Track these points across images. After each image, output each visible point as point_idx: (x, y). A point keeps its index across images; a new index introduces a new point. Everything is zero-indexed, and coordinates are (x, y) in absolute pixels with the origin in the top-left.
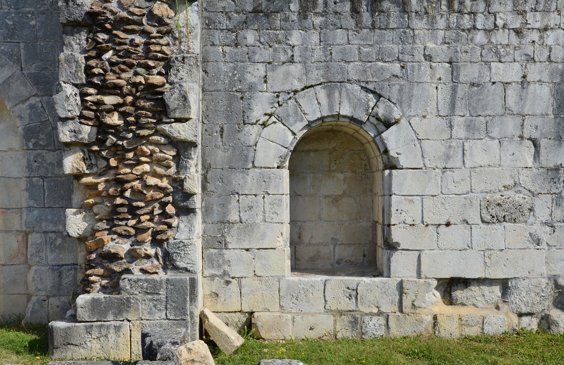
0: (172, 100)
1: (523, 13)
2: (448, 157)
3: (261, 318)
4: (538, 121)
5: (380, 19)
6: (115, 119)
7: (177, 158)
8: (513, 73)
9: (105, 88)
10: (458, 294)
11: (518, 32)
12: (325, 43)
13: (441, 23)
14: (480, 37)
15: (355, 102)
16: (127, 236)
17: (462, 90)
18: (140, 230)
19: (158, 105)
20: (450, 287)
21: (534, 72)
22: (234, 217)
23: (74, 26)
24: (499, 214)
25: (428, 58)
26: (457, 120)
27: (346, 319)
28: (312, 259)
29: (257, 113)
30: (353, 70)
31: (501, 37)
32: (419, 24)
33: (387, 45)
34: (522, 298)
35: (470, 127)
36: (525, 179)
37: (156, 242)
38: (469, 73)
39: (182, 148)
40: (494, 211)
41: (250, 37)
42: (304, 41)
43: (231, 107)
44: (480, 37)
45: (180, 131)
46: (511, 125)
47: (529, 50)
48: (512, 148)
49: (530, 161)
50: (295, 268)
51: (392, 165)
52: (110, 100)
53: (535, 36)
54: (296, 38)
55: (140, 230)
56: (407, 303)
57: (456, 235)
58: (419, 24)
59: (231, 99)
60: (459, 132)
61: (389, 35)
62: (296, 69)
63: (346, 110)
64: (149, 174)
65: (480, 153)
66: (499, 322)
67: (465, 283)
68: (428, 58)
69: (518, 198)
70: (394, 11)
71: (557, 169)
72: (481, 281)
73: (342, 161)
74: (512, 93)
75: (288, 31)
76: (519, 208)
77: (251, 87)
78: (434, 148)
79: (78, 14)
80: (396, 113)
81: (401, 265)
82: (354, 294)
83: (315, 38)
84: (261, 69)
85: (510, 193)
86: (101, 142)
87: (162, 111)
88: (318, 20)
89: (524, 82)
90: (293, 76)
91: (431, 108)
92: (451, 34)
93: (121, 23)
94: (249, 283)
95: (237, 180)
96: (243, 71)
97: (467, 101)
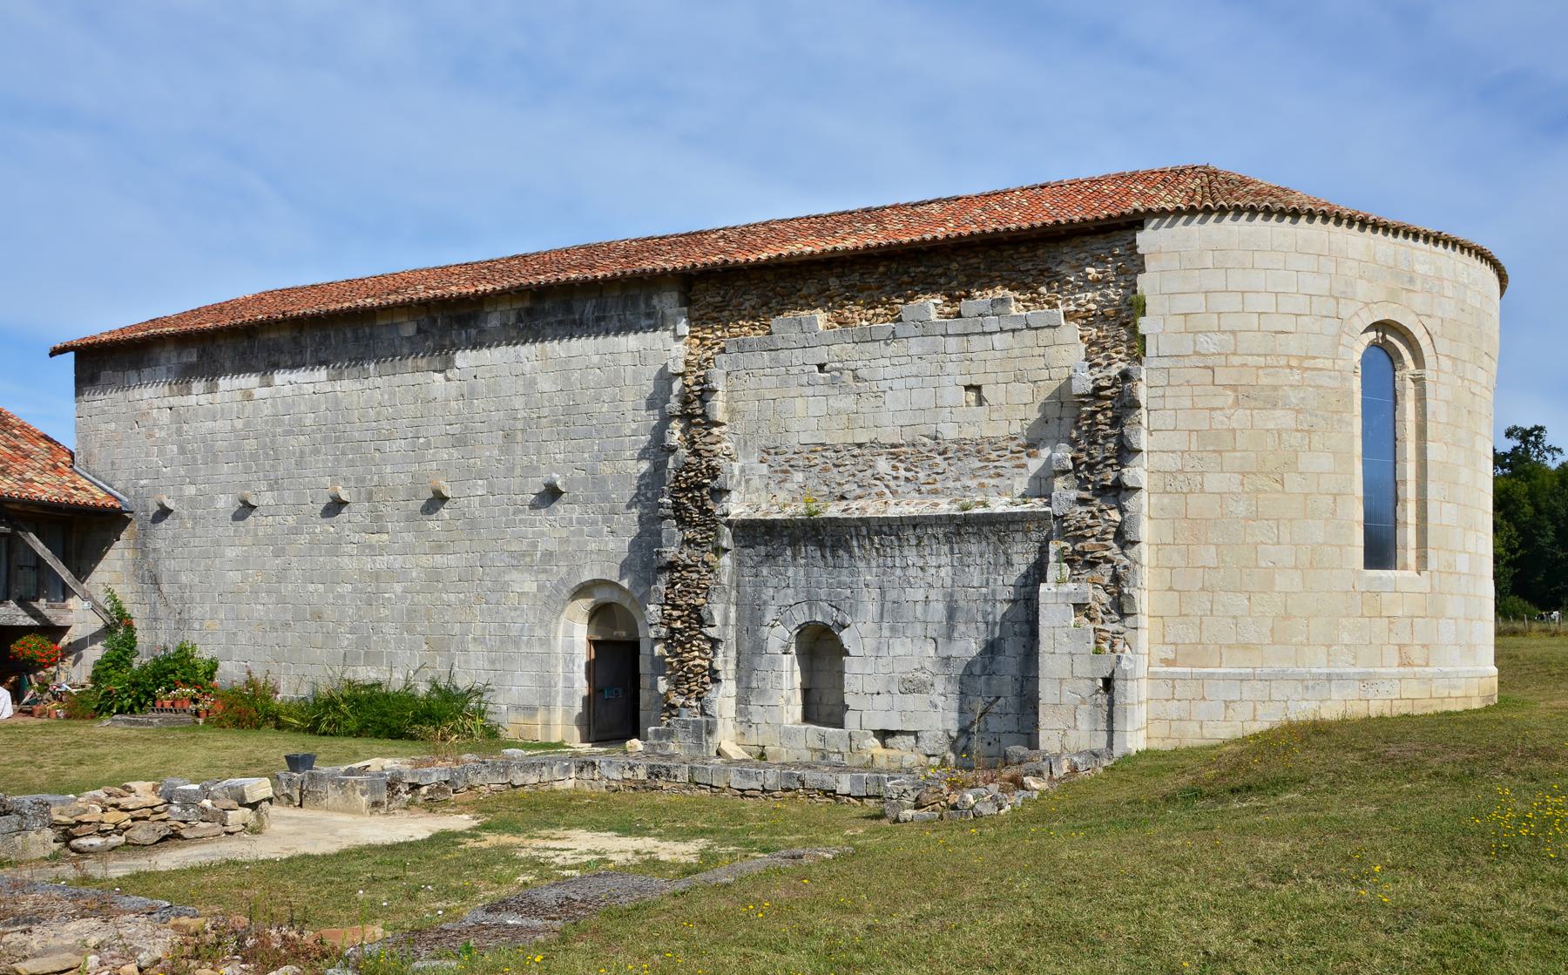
0: (704, 614)
1: (923, 557)
2: (878, 649)
3: (769, 749)
4: (937, 626)
5: (838, 562)
6: (678, 625)
7: (712, 648)
8: (920, 595)
9: (675, 607)
10: (889, 741)
11: (922, 569)
12: (807, 575)
13: (874, 563)
14: (898, 572)
15: (824, 614)
16: (682, 694)
17: (888, 605)
18: (690, 691)
19: (698, 618)
20: (884, 735)
21: (933, 595)
22: (754, 685)
23: (661, 569)
24: (912, 687)
25: (867, 586)
26: (885, 625)
27: (819, 754)
28: (829, 715)
29: (768, 619)
30: (823, 593)
31: (912, 572)
32: (861, 565)
33: (843, 578)
34: (927, 744)
35: (893, 629)
36: (927, 664)
37: (698, 699)
38: (892, 595)
39: (714, 643)
40: (907, 685)
41: (765, 571)
42: (796, 574)
43: (751, 618)
44: (898, 572)
45: (712, 632)
46: (919, 628)
47: (930, 580)
48: (919, 643)
49: (932, 652)
50: (807, 717)
51: (847, 653)
52: (676, 613)
53: (933, 571)
54: (791, 572)
55: (690, 691)
56: (854, 746)
57: (882, 701)
58: (861, 565)
59: (753, 610)
60: (886, 632)
61: (845, 572)
62: (790, 591)
63: (819, 618)
64: (696, 659)
65: (900, 647)
66: (911, 759)
67: (893, 733)
68: (867, 586)
69: (923, 677)
70: (846, 556)
71: (948, 658)
72: (902, 733)
73: (820, 648)
74: (919, 608)
75: (786, 567)
76: (924, 684)
77: (765, 603)
78: (870, 642)
79: (663, 563)
80: (849, 620)
81: (851, 719)
82: (823, 738)
83: (802, 573)
84: (771, 591)
85: (919, 674)
86: (672, 638)
87: (701, 621)
88: (803, 561)
89: (927, 600)
90: (789, 596)
91: (869, 617)
92: (881, 570)
93: (686, 567)
94: (762, 727)
95: (756, 660)
96: (760, 592)
97: (893, 615)
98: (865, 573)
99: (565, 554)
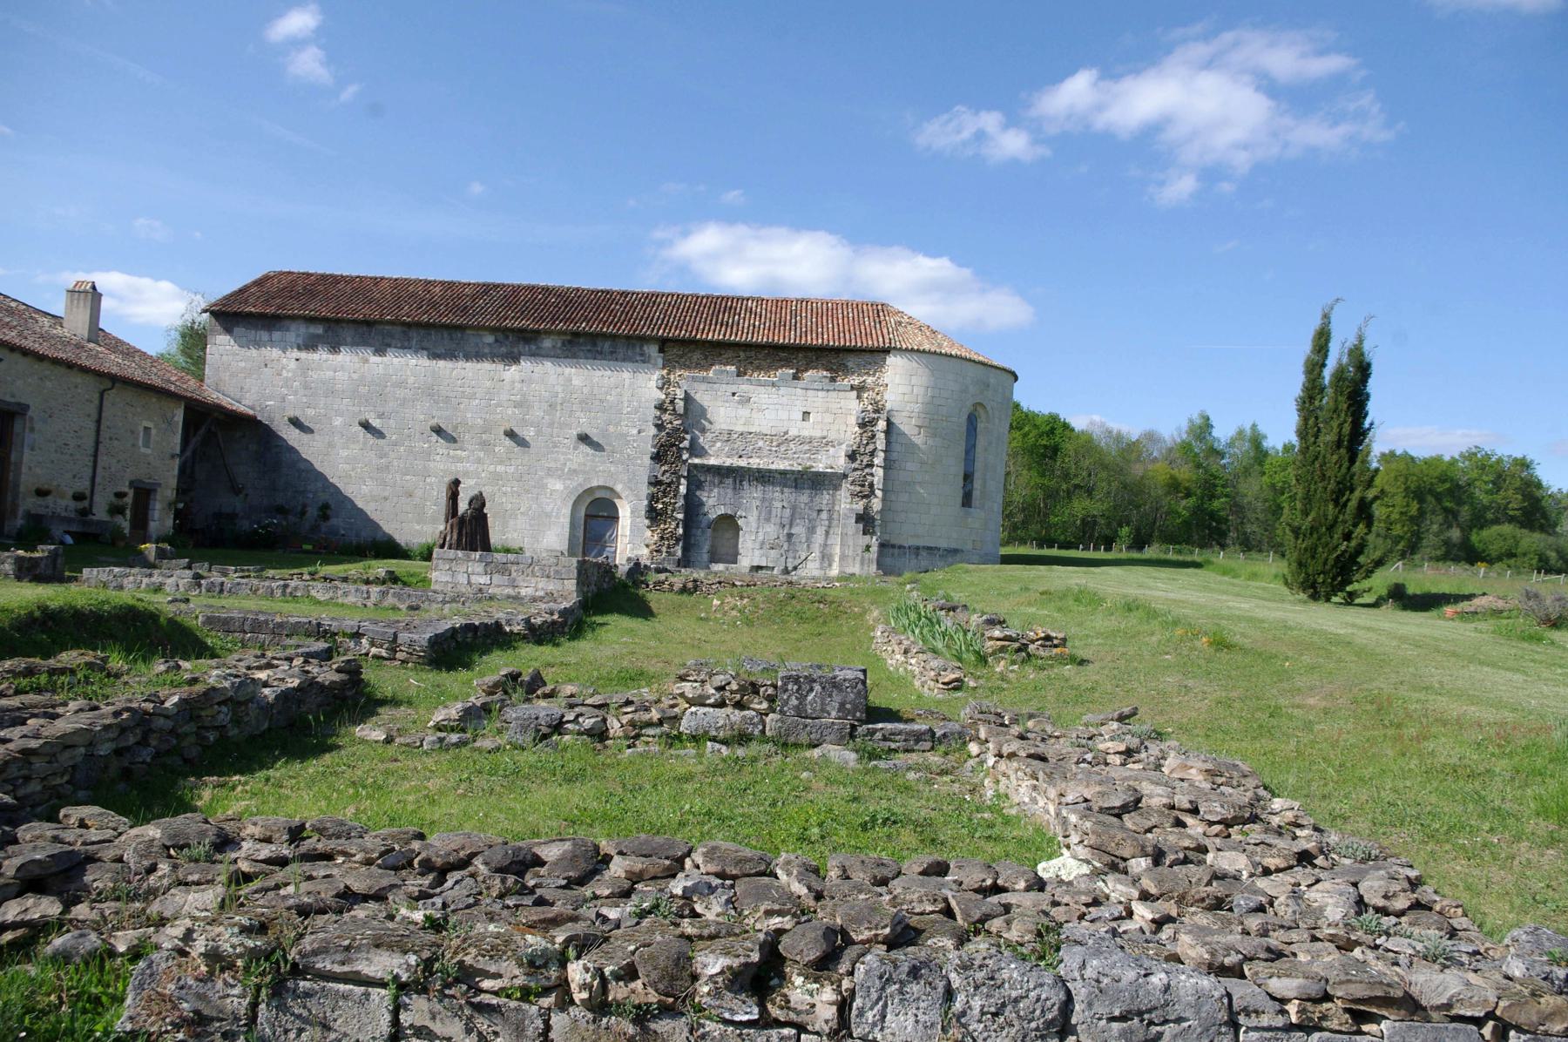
98: (753, 495)
99: (584, 472)
